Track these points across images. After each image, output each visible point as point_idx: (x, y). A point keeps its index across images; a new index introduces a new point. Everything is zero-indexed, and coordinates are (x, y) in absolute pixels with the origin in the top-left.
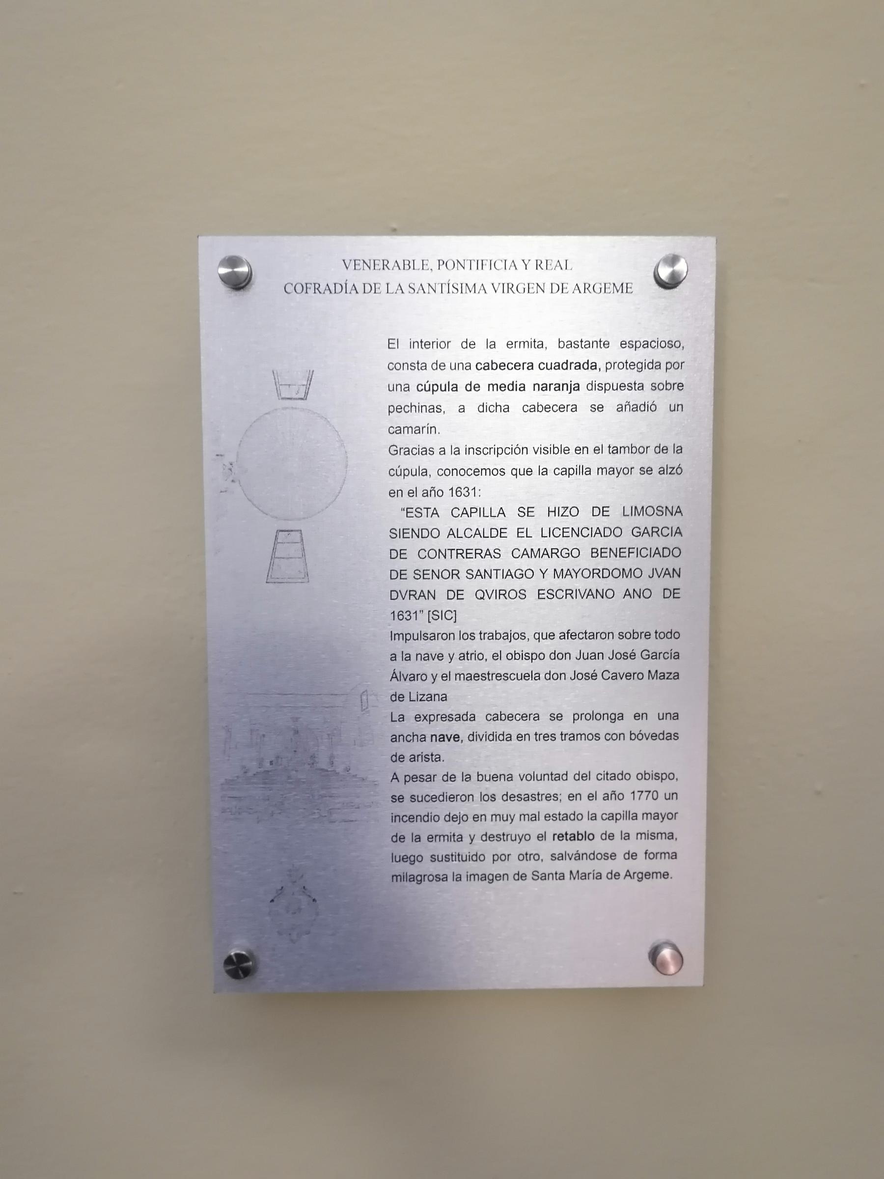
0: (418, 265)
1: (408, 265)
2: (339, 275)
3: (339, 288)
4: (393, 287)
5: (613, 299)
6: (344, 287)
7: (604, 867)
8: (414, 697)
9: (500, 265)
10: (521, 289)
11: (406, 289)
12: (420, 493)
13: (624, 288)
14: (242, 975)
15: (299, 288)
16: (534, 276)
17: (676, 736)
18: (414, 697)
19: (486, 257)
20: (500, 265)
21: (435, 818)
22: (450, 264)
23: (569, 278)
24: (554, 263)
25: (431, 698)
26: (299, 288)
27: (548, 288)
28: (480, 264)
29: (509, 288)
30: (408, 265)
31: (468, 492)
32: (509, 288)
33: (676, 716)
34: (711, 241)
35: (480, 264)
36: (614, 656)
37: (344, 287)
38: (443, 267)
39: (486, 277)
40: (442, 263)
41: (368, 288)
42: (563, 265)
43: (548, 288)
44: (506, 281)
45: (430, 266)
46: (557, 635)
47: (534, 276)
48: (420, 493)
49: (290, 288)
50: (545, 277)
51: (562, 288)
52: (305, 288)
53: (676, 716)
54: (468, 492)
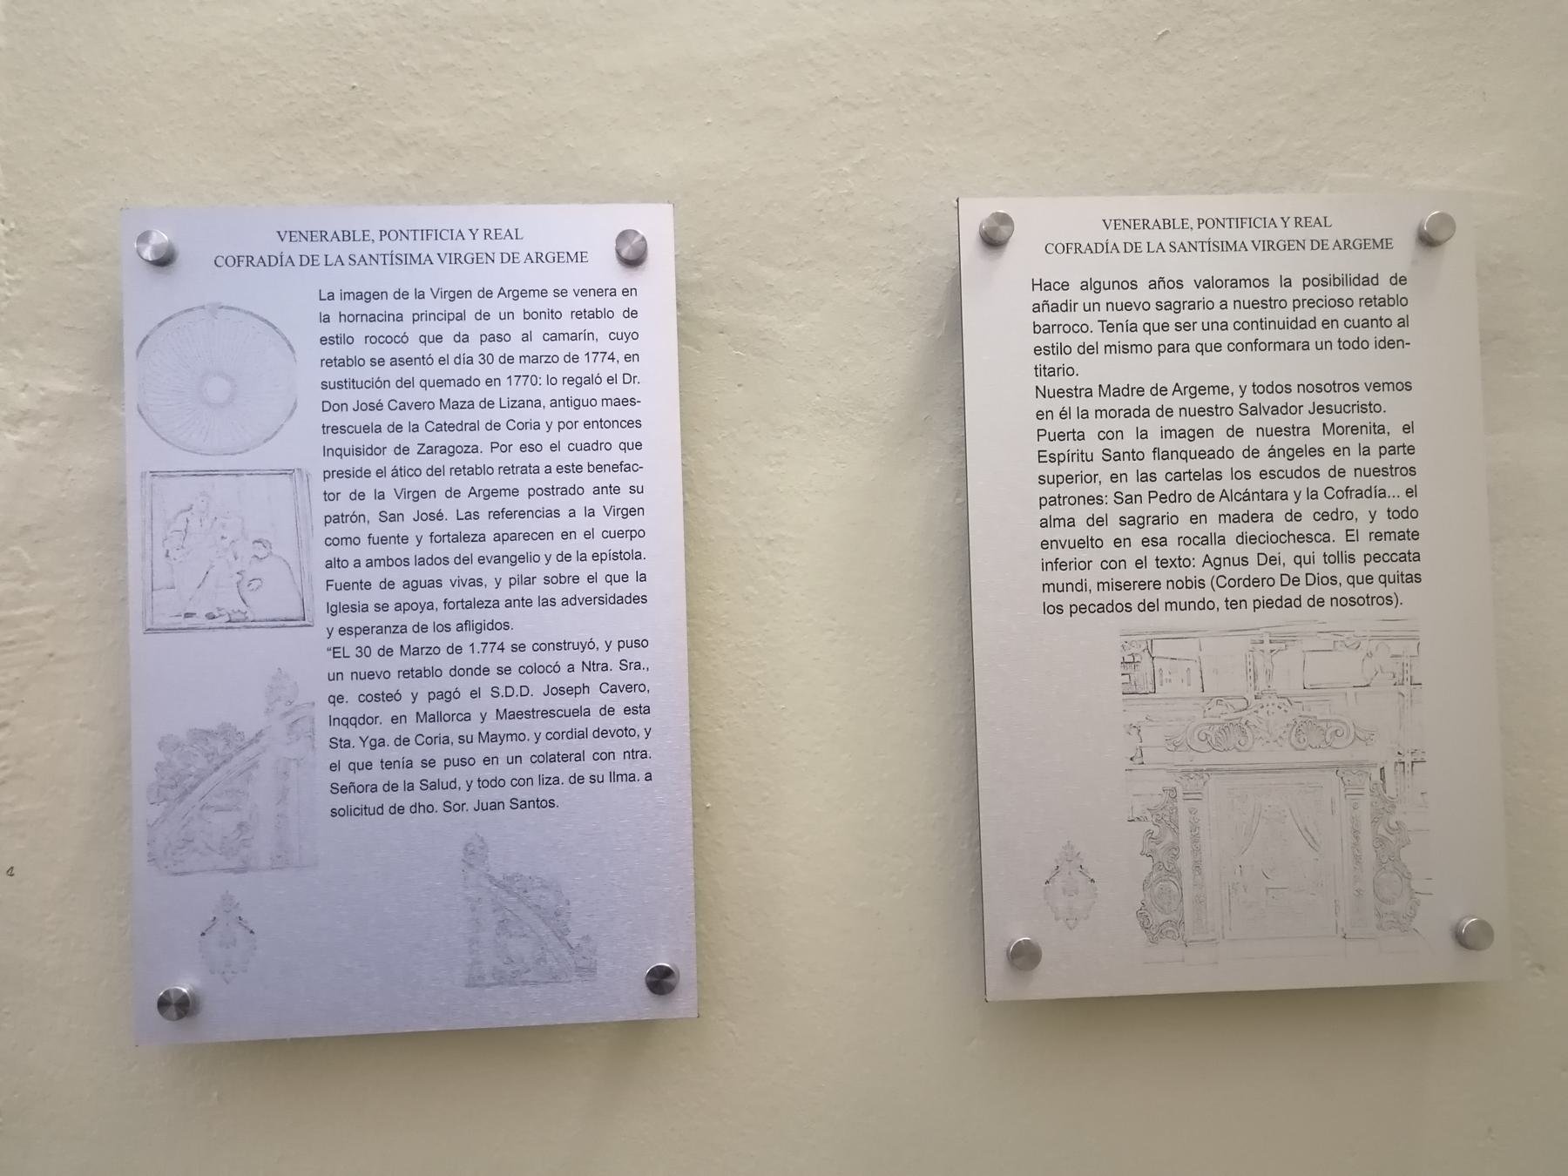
0: (359, 236)
1: (1169, 224)
2: (276, 247)
3: (273, 261)
4: (1153, 247)
8: (504, 404)
12: (389, 473)
14: (175, 1014)
15: (230, 261)
17: (644, 599)
18: (504, 404)
20: (446, 235)
21: (608, 446)
22: (1210, 223)
23: (523, 249)
24: (504, 232)
25: (523, 404)
26: (230, 261)
27: (498, 258)
33: (334, 813)
37: (1105, 247)
38: (385, 238)
39: (1246, 235)
40: (384, 234)
42: (513, 235)
43: (498, 258)
46: (453, 627)
47: (481, 245)
48: (389, 473)
49: (220, 262)
51: (1322, 245)
53: (334, 813)
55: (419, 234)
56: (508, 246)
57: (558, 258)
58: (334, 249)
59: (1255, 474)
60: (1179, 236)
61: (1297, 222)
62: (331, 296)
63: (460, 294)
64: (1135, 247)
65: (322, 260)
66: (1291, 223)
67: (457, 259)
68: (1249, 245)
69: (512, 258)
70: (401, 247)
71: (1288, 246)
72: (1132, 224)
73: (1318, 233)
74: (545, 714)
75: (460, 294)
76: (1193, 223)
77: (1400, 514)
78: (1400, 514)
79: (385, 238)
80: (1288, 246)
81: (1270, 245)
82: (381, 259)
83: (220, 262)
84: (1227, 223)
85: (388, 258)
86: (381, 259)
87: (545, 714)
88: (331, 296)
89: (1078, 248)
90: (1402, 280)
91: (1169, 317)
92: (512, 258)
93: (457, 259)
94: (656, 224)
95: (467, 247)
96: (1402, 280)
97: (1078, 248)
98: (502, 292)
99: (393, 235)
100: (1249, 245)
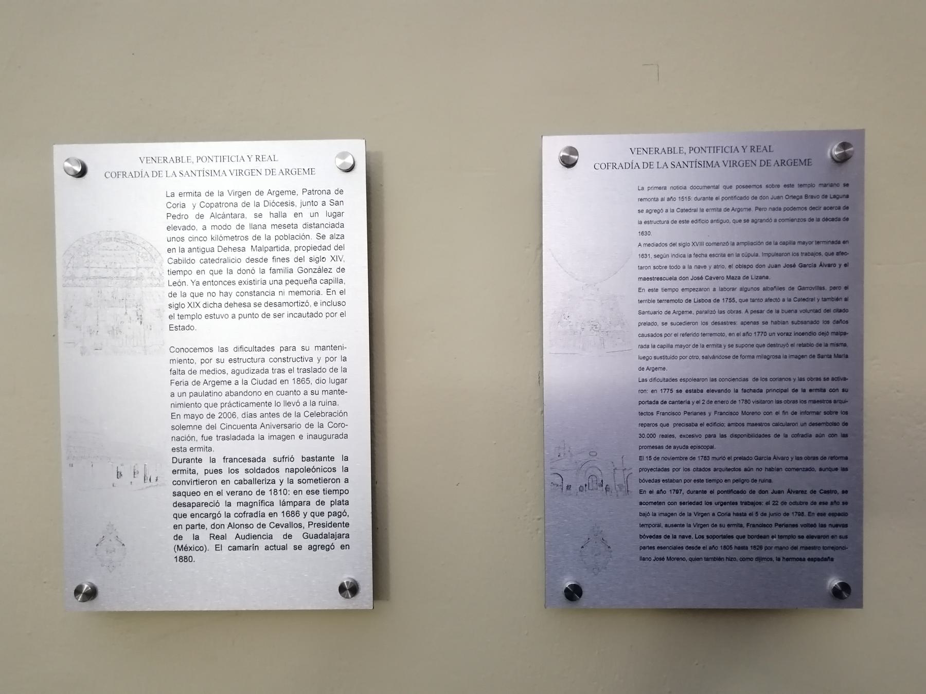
0: (185, 159)
1: (179, 160)
2: (139, 167)
3: (137, 174)
5: (802, 168)
6: (141, 174)
7: (304, 310)
9: (728, 150)
11: (669, 165)
15: (113, 175)
16: (254, 164)
20: (728, 150)
22: (204, 159)
23: (277, 166)
24: (762, 148)
26: (113, 175)
27: (263, 172)
28: (223, 159)
30: (179, 160)
34: (55, 146)
35: (223, 159)
36: (694, 278)
37: (141, 174)
38: (200, 161)
39: (226, 166)
40: (199, 158)
45: (684, 151)
47: (254, 164)
49: (108, 175)
50: (262, 166)
51: (767, 163)
55: (712, 149)
58: (171, 167)
59: (270, 260)
60: (185, 167)
61: (752, 149)
62: (173, 195)
64: (650, 165)
65: (655, 165)
66: (748, 149)
68: (721, 164)
71: (251, 173)
72: (648, 151)
74: (240, 305)
76: (686, 150)
80: (251, 173)
81: (240, 173)
82: (689, 164)
84: (214, 159)
85: (201, 173)
86: (689, 164)
87: (240, 305)
88: (173, 195)
89: (124, 174)
90: (341, 192)
94: (553, 147)
96: (341, 192)
97: (614, 167)
99: (697, 150)
100: (721, 164)
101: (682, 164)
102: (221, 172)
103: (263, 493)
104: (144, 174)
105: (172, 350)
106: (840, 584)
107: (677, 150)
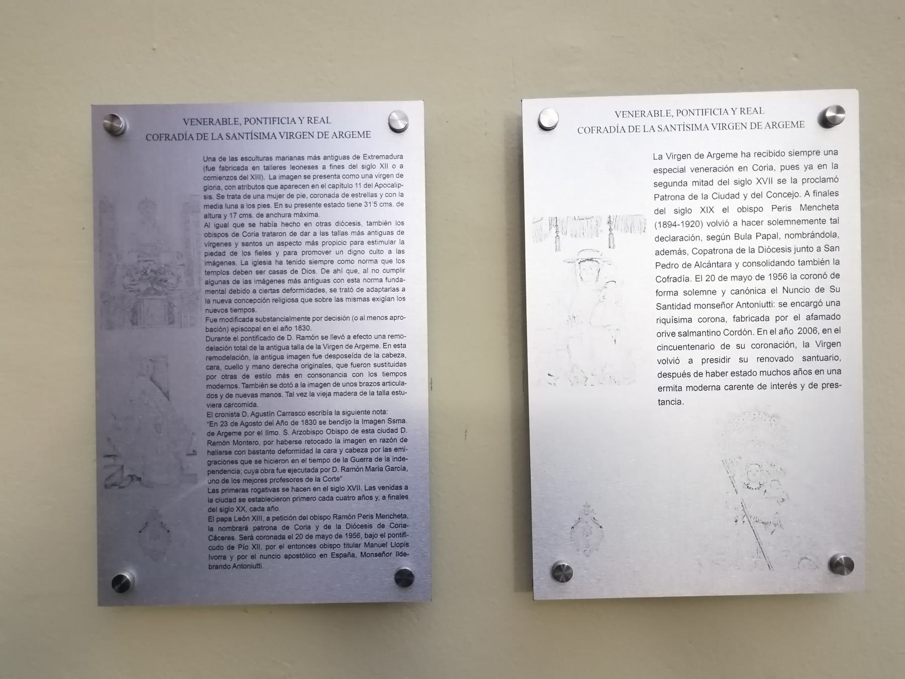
1: (658, 114)
2: (183, 128)
3: (613, 129)
4: (216, 136)
6: (184, 136)
9: (717, 112)
10: (731, 127)
11: (656, 129)
12: (778, 332)
13: (799, 124)
15: (587, 130)
16: (739, 118)
19: (639, 108)
20: (717, 112)
22: (685, 112)
23: (763, 119)
24: (753, 110)
26: (587, 130)
28: (704, 112)
29: (723, 126)
30: (658, 114)
31: (306, 328)
32: (723, 126)
35: (704, 112)
37: (616, 129)
38: (248, 123)
39: (708, 120)
40: (680, 112)
41: (631, 129)
43: (316, 135)
44: (721, 122)
47: (739, 118)
48: (778, 332)
49: (150, 137)
50: (747, 119)
51: (758, 125)
52: (160, 137)
54: (306, 328)
55: (268, 120)
56: (322, 127)
57: (352, 135)
60: (664, 121)
61: (742, 111)
62: (661, 157)
63: (684, 156)
64: (636, 129)
65: (210, 136)
66: (738, 112)
67: (291, 135)
69: (325, 135)
70: (690, 120)
71: (735, 127)
72: (634, 114)
73: (756, 118)
75: (684, 156)
76: (674, 113)
77: (698, 388)
78: (698, 388)
79: (248, 123)
82: (677, 128)
83: (581, 130)
85: (249, 136)
91: (237, 192)
92: (325, 135)
93: (291, 135)
95: (296, 128)
98: (710, 155)
101: (237, 136)
102: (271, 135)
103: (297, 423)
104: (188, 136)
105: (659, 279)
106: (128, 581)
107: (664, 113)
